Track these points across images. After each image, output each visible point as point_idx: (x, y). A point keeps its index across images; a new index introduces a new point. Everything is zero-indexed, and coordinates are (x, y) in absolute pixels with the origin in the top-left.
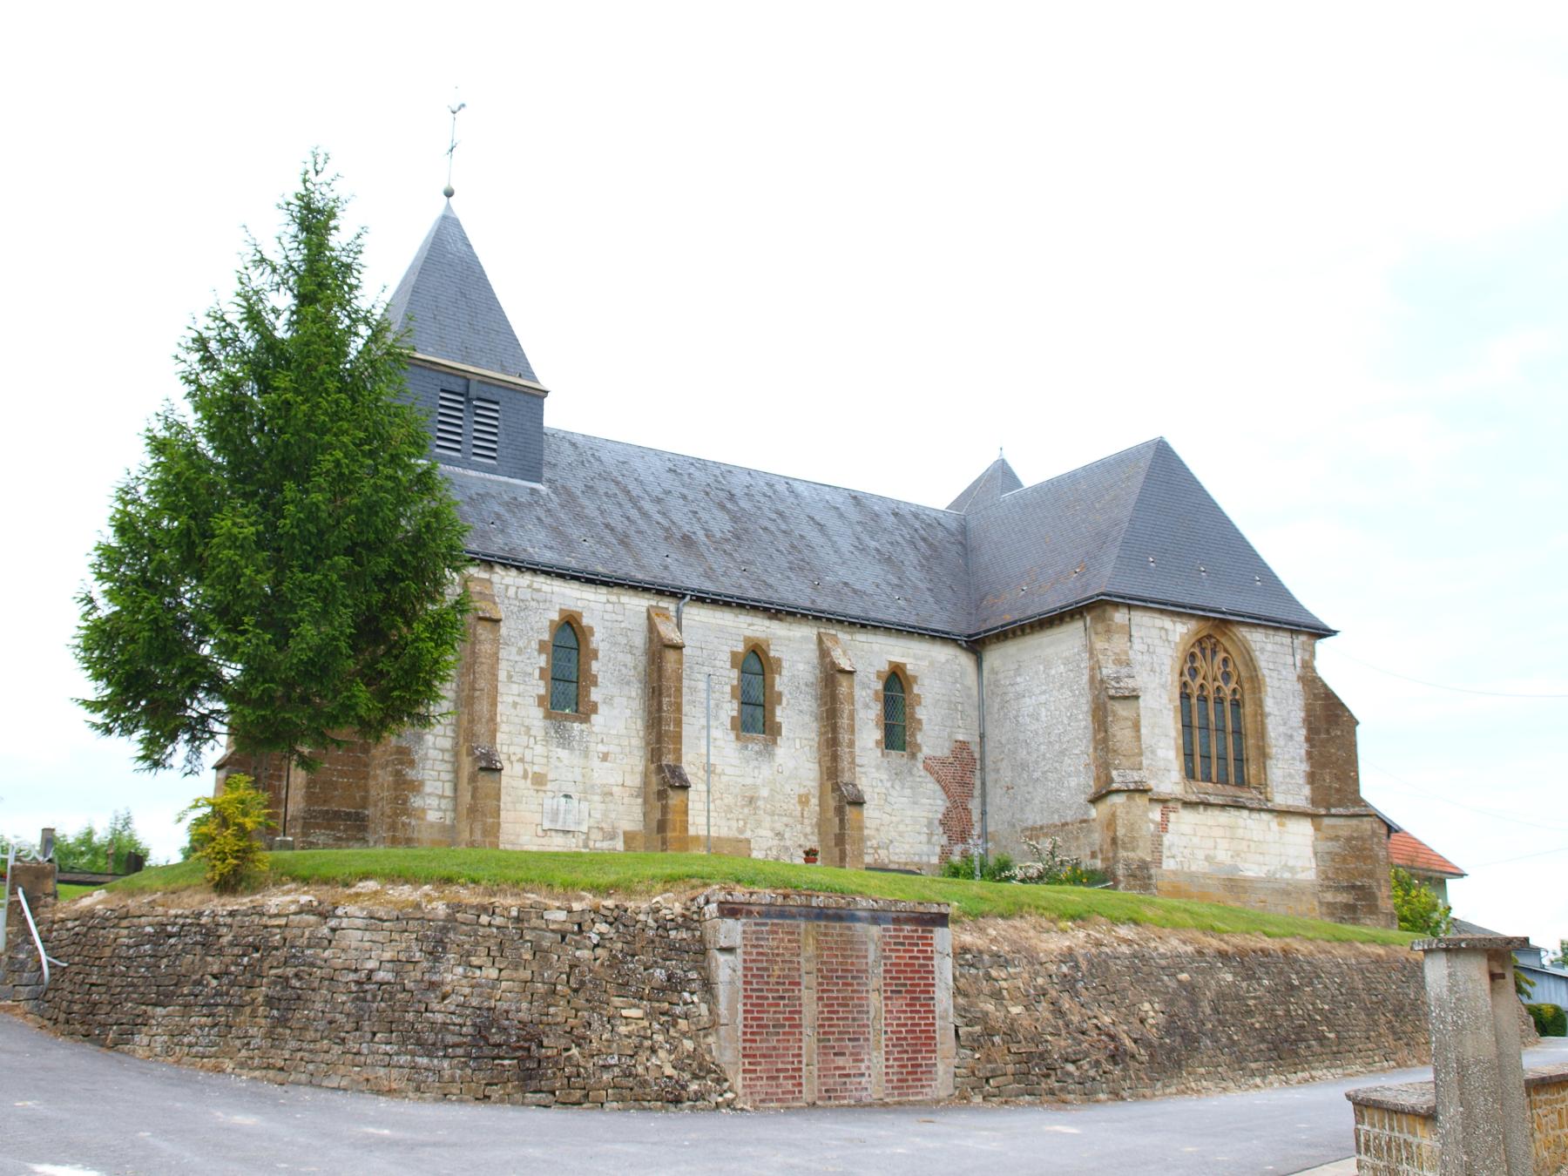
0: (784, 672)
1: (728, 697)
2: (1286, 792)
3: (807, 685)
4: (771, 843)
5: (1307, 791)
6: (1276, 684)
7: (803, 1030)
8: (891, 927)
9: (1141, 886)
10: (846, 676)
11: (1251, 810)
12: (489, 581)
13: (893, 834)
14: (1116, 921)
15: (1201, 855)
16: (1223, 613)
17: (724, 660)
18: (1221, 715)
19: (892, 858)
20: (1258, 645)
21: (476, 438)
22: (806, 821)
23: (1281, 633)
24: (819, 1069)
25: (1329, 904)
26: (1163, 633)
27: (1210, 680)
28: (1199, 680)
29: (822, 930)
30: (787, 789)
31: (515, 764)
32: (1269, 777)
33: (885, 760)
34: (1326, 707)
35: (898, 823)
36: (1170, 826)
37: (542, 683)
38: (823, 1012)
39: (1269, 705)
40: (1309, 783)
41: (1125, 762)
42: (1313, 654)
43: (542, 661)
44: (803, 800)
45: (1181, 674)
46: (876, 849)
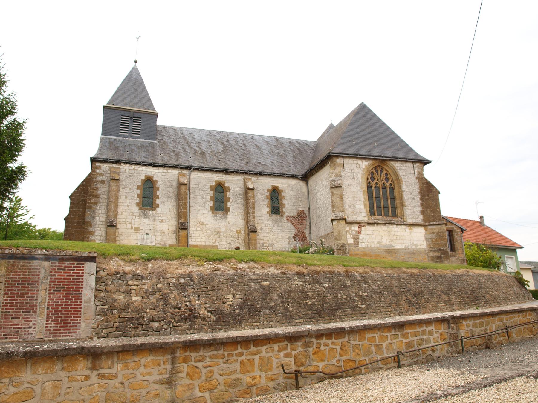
1: (209, 200)
2: (412, 218)
4: (226, 246)
5: (421, 217)
6: (407, 180)
8: (57, 262)
10: (251, 191)
11: (397, 225)
13: (274, 242)
14: (240, 261)
15: (376, 241)
16: (382, 157)
17: (207, 188)
19: (274, 250)
20: (399, 168)
22: (240, 239)
23: (408, 163)
25: (431, 256)
26: (358, 165)
27: (380, 181)
28: (375, 181)
29: (11, 263)
31: (128, 225)
32: (405, 213)
33: (271, 218)
34: (427, 187)
35: (276, 238)
36: (362, 232)
37: (138, 199)
38: (7, 300)
39: (404, 188)
40: (422, 214)
42: (422, 170)
43: (138, 192)
44: (238, 232)
45: (368, 180)
46: (267, 247)
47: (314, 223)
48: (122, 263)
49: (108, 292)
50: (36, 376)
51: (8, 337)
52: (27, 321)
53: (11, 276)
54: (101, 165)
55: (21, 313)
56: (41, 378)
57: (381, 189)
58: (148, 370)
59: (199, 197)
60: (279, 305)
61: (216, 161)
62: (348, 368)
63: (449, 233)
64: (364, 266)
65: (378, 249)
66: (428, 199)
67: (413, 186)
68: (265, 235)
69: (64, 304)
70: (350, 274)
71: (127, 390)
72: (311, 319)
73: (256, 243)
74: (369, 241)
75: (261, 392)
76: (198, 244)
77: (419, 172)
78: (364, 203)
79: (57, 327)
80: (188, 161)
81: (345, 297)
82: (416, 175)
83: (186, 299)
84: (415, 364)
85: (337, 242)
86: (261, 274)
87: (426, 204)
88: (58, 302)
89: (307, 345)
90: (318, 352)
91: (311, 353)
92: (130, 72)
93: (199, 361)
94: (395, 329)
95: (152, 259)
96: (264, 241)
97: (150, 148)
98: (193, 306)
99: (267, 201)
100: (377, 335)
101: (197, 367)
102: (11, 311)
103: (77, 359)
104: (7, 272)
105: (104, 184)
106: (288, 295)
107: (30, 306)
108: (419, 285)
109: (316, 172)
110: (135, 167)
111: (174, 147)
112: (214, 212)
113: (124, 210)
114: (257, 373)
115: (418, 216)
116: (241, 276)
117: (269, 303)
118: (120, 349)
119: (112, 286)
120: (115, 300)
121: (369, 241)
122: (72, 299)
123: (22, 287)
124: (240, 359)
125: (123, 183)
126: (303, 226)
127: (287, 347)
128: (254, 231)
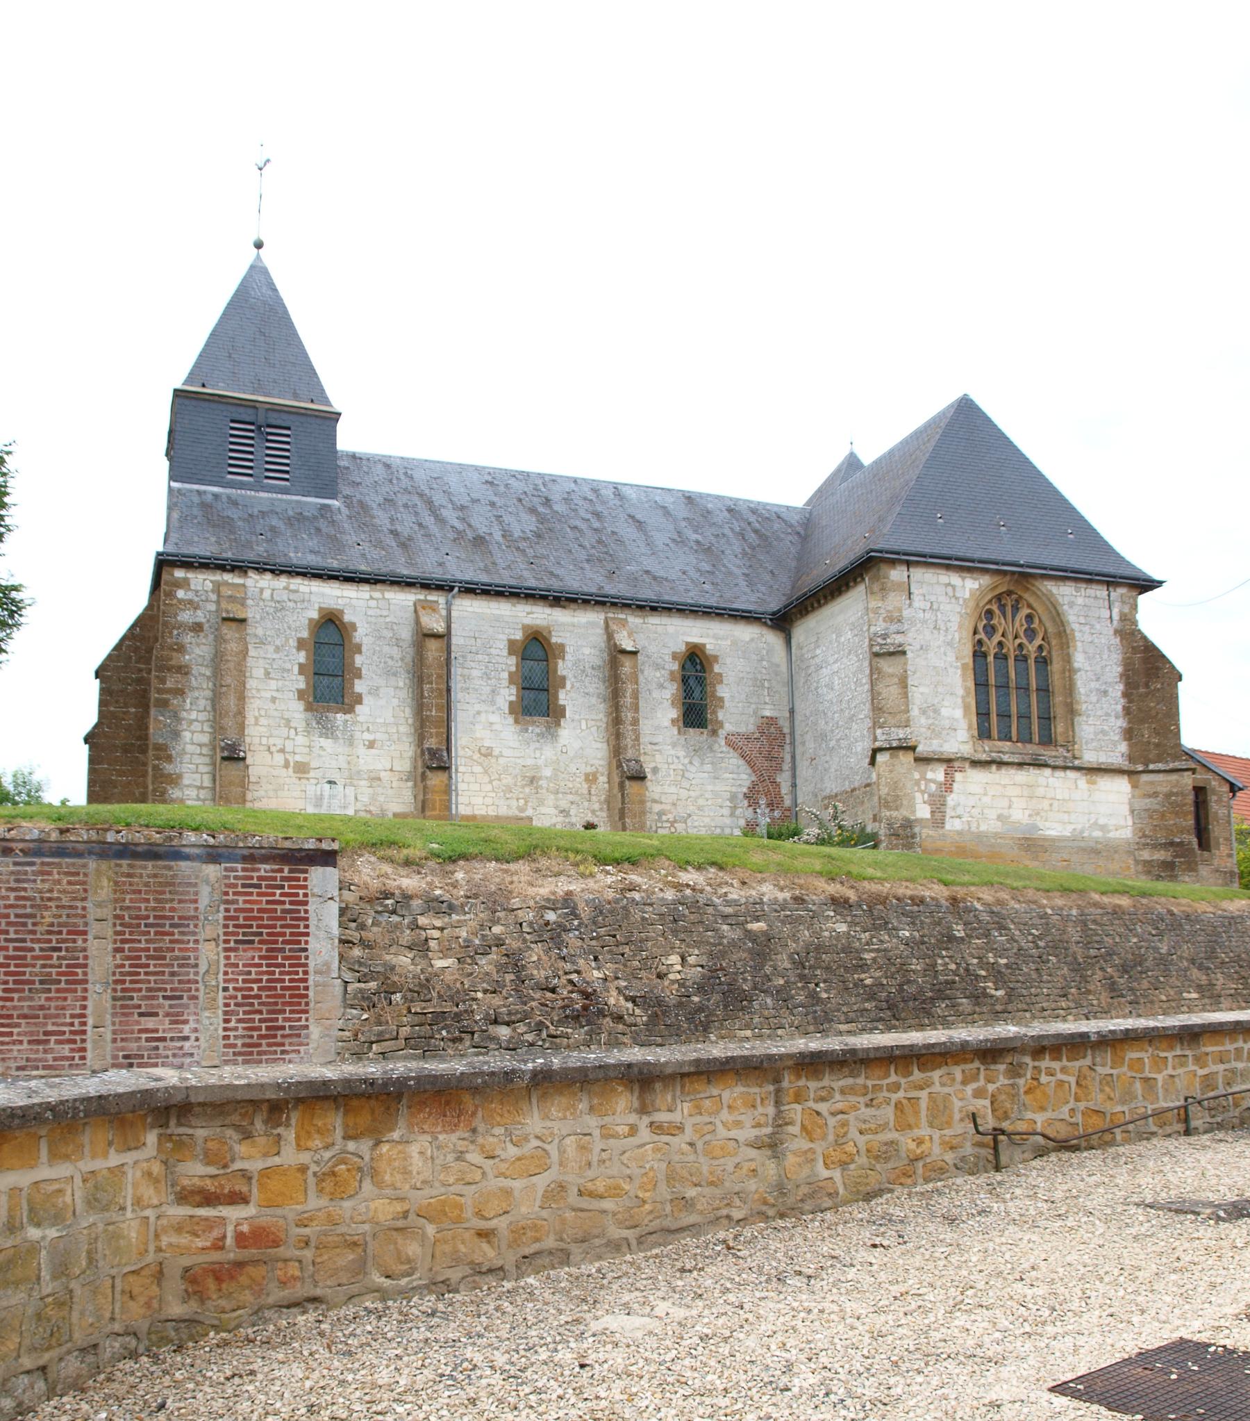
0: (568, 657)
3: (593, 668)
4: (554, 820)
5: (1123, 747)
6: (1088, 638)
7: (89, 986)
8: (239, 866)
9: (903, 845)
10: (628, 657)
11: (1055, 768)
12: (244, 585)
14: (684, 865)
15: (992, 814)
16: (1022, 566)
17: (501, 647)
18: (1023, 673)
21: (267, 463)
22: (594, 798)
23: (1094, 586)
24: (114, 1032)
25: (1146, 862)
26: (950, 589)
27: (1010, 637)
28: (997, 638)
29: (125, 869)
30: (573, 768)
31: (276, 755)
33: (683, 738)
34: (1146, 660)
35: (697, 798)
36: (955, 786)
37: (302, 678)
38: (123, 966)
39: (1079, 660)
40: (1125, 740)
41: (891, 721)
42: (1135, 607)
43: (302, 657)
44: (591, 779)
45: (975, 633)
46: (672, 823)
47: (808, 756)
48: (387, 868)
49: (370, 947)
50: (549, 1124)
51: (135, 1061)
52: (176, 1022)
53: (127, 903)
54: (190, 575)
55: (161, 1000)
56: (557, 1126)
57: (1011, 662)
58: (735, 1116)
59: (475, 673)
60: (795, 983)
61: (523, 566)
62: (1090, 1130)
63: (1197, 796)
64: (992, 885)
65: (996, 835)
66: (1147, 694)
67: (1105, 657)
68: (667, 789)
69: (265, 977)
70: (961, 905)
71: (702, 1159)
72: (875, 1024)
73: (643, 813)
74: (975, 812)
75: (933, 1175)
76: (477, 812)
77: (1126, 615)
78: (963, 702)
79: (252, 1037)
80: (440, 565)
81: (953, 967)
82: (1115, 623)
83: (568, 967)
84: (1218, 1129)
85: (888, 814)
86: (743, 901)
87: (1139, 709)
88: (249, 973)
89: (1015, 1071)
90: (1035, 1087)
91: (1022, 1091)
92: (245, 279)
93: (823, 1099)
94: (1182, 1044)
95: (464, 857)
96: (663, 807)
97: (322, 524)
98: (588, 983)
99: (671, 690)
100: (1144, 1054)
101: (818, 1113)
102: (135, 995)
103: (613, 1090)
104: (115, 891)
105: (202, 634)
106: (816, 959)
107: (180, 982)
108: (1135, 940)
109: (820, 606)
110: (289, 584)
111: (392, 520)
112: (521, 718)
113: (263, 713)
114: (924, 1131)
115: (1115, 744)
116: (694, 906)
117: (770, 980)
118: (692, 1069)
119: (375, 929)
120: (393, 968)
121: (975, 812)
122: (284, 966)
123: (156, 933)
124: (895, 1097)
125: (257, 629)
126: (774, 764)
127: (978, 1074)
128: (640, 777)
